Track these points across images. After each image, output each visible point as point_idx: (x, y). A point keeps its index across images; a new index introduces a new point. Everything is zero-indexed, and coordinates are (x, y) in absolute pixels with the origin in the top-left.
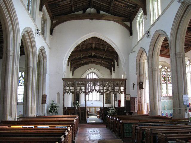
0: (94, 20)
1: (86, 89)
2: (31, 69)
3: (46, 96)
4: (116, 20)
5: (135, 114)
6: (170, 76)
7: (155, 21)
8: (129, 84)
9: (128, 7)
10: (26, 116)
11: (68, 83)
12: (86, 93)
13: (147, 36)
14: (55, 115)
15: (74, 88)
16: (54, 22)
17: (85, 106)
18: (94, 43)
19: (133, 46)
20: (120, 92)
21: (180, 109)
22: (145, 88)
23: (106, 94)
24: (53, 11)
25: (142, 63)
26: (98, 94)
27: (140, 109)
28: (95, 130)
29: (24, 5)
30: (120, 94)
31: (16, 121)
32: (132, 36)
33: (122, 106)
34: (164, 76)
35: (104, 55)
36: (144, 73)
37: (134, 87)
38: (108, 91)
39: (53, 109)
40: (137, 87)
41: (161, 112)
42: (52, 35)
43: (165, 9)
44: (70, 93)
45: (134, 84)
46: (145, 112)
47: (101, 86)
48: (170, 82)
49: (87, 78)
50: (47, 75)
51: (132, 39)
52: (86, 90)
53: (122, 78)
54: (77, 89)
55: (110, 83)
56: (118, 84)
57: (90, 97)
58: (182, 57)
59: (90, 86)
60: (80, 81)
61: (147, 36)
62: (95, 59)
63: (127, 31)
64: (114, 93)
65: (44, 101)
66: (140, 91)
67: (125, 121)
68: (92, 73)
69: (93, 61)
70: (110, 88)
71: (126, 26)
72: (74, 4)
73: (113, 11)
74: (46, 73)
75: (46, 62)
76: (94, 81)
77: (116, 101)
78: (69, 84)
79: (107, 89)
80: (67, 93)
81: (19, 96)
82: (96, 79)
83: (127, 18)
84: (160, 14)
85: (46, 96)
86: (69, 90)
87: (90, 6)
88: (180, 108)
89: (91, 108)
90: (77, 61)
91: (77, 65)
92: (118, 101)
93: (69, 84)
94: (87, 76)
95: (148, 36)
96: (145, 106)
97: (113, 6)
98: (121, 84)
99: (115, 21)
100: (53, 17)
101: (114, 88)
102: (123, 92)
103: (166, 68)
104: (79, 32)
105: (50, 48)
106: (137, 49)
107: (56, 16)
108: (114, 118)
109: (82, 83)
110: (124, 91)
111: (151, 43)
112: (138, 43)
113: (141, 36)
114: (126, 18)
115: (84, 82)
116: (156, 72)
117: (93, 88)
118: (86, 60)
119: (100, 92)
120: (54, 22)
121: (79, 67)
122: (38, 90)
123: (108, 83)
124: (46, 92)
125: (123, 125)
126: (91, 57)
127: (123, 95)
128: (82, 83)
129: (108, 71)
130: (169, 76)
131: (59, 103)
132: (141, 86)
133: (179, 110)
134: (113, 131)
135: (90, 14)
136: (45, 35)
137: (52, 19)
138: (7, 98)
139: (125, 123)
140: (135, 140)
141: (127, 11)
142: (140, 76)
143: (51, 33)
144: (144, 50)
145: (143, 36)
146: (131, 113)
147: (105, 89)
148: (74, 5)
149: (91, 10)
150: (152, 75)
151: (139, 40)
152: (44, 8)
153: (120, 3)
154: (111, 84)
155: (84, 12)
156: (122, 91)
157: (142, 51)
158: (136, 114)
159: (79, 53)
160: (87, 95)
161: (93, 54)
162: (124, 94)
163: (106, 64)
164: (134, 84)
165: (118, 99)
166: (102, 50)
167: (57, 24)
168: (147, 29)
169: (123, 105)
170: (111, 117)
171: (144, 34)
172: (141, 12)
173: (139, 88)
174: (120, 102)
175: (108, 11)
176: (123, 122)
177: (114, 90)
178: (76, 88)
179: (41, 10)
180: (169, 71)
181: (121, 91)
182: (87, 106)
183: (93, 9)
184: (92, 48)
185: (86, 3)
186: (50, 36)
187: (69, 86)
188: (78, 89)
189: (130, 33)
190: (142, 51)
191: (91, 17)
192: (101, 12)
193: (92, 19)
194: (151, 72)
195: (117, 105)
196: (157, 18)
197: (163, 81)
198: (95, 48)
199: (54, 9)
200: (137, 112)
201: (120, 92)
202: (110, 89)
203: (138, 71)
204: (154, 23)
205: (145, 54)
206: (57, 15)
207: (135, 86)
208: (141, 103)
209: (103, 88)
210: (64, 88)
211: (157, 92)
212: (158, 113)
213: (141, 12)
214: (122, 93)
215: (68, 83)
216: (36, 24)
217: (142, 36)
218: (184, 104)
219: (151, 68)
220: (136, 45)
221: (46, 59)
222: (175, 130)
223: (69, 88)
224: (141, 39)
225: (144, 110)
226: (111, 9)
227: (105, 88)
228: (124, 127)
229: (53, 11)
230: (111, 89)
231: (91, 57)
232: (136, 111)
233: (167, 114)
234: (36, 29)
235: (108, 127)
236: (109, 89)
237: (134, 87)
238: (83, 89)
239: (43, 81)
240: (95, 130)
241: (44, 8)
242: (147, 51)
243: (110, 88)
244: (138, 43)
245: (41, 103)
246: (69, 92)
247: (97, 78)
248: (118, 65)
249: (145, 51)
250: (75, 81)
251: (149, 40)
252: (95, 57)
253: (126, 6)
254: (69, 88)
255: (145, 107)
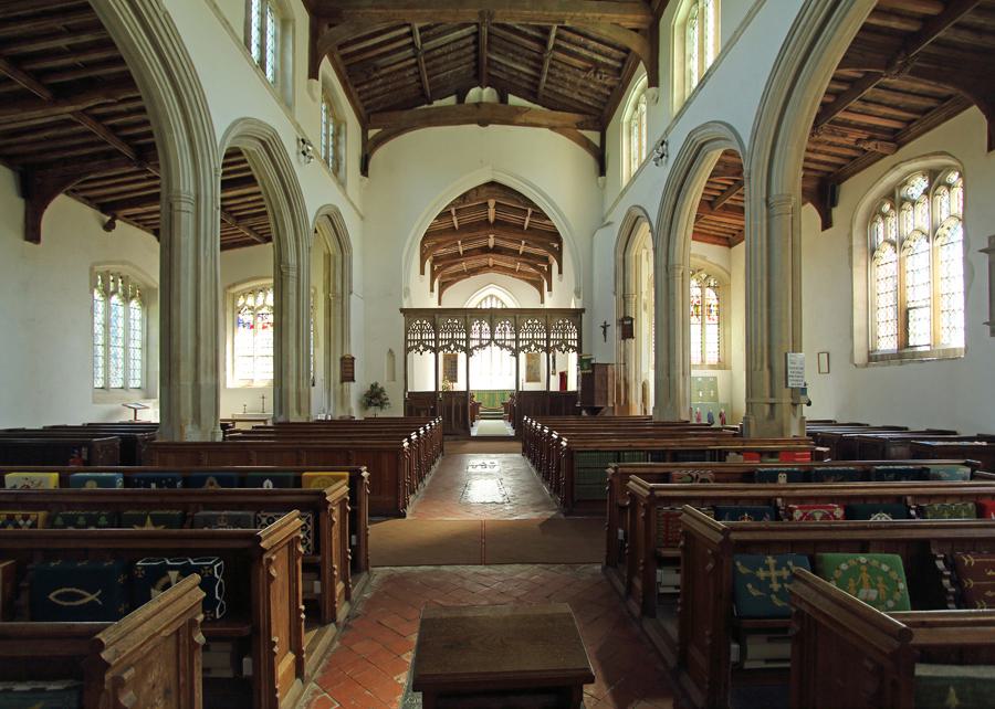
0: (490, 126)
2: (293, 273)
3: (353, 358)
4: (558, 123)
5: (606, 415)
7: (690, 98)
9: (595, 73)
10: (281, 419)
12: (469, 352)
13: (656, 160)
16: (372, 133)
17: (465, 389)
18: (492, 203)
19: (607, 209)
21: (772, 405)
22: (638, 335)
24: (366, 95)
26: (506, 353)
28: (488, 462)
29: (232, 32)
31: (218, 443)
35: (523, 242)
36: (638, 292)
37: (605, 332)
38: (530, 345)
39: (374, 396)
40: (614, 331)
42: (367, 176)
43: (738, 29)
44: (424, 350)
46: (636, 411)
50: (353, 297)
52: (467, 343)
53: (573, 307)
54: (442, 340)
56: (559, 325)
58: (790, 211)
59: (479, 330)
61: (656, 160)
62: (499, 256)
63: (589, 160)
64: (548, 350)
65: (348, 375)
67: (578, 446)
69: (494, 265)
71: (586, 144)
72: (427, 69)
73: (550, 90)
74: (351, 293)
75: (350, 258)
77: (554, 374)
79: (529, 340)
81: (122, 344)
83: (592, 119)
84: (710, 60)
85: (353, 358)
86: (421, 341)
87: (478, 79)
88: (773, 401)
89: (910, 312)
95: (661, 157)
97: (551, 66)
99: (552, 128)
100: (369, 116)
101: (548, 336)
102: (573, 347)
103: (704, 276)
104: (445, 161)
105: (362, 218)
106: (618, 217)
107: (377, 112)
108: (542, 428)
111: (668, 181)
112: (622, 195)
113: (635, 167)
114: (588, 117)
117: (488, 337)
118: (474, 262)
120: (372, 133)
123: (561, 322)
126: (485, 250)
127: (573, 357)
132: (628, 331)
133: (767, 408)
134: (539, 470)
135: (478, 105)
137: (365, 124)
138: (179, 365)
139: (578, 452)
140: (621, 531)
141: (592, 90)
142: (624, 298)
143: (364, 170)
144: (640, 213)
145: (642, 166)
146: (594, 411)
147: (523, 340)
148: (430, 72)
149: (481, 95)
150: (668, 294)
151: (625, 182)
152: (326, 66)
153: (571, 59)
155: (461, 100)
156: (571, 346)
157: (632, 225)
159: (452, 237)
165: (559, 369)
167: (379, 141)
168: (658, 137)
169: (572, 386)
171: (644, 157)
172: (641, 80)
173: (620, 336)
174: (564, 377)
175: (532, 95)
177: (548, 344)
179: (314, 73)
180: (712, 284)
183: (488, 89)
185: (465, 66)
187: (421, 330)
189: (598, 167)
190: (632, 225)
191: (483, 116)
192: (513, 100)
193: (483, 123)
195: (555, 386)
196: (695, 84)
199: (366, 87)
200: (613, 408)
201: (563, 347)
203: (620, 286)
204: (686, 104)
205: (645, 227)
206: (382, 111)
207: (608, 329)
208: (625, 379)
209: (517, 336)
213: (641, 80)
215: (418, 322)
216: (298, 119)
217: (637, 168)
218: (790, 384)
221: (350, 248)
222: (248, 209)
224: (633, 179)
225: (634, 402)
226: (541, 88)
229: (366, 95)
230: (540, 340)
231: (485, 250)
232: (610, 405)
233: (710, 416)
234: (298, 140)
235: (526, 451)
237: (605, 332)
238: (460, 340)
239: (342, 316)
241: (326, 66)
242: (654, 217)
244: (625, 190)
246: (421, 348)
247: (499, 307)
249: (647, 215)
250: (437, 316)
251: (663, 172)
252: (497, 250)
253: (587, 70)
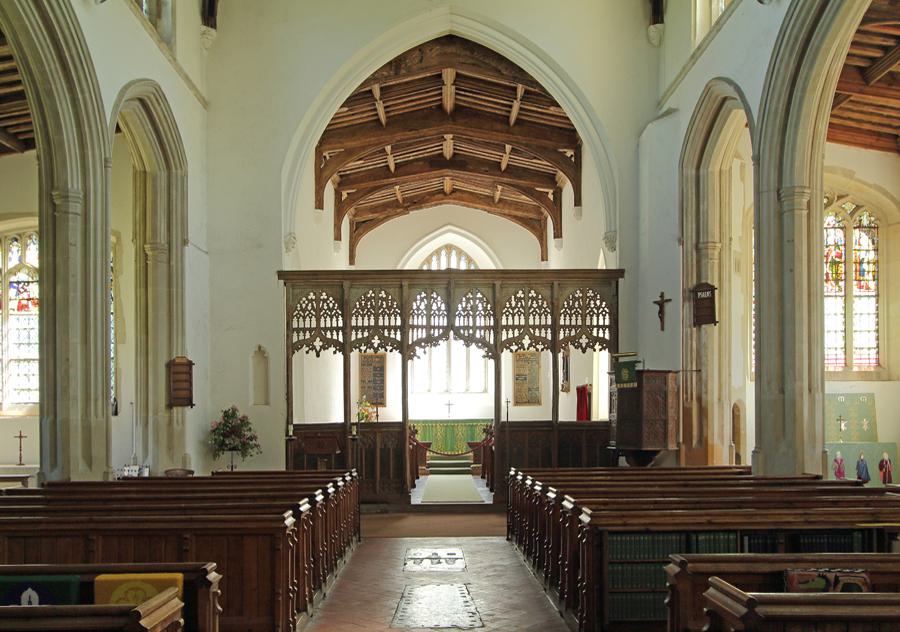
1: (404, 328)
3: (190, 364)
5: (664, 465)
6: (872, 256)
8: (638, 299)
10: (54, 476)
11: (312, 296)
14: (245, 465)
15: (404, 321)
18: (449, 75)
20: (584, 341)
22: (725, 316)
23: (519, 359)
25: (717, 174)
27: (695, 432)
28: (442, 553)
30: (584, 351)
32: (662, 22)
33: (594, 418)
34: (833, 254)
37: (661, 313)
38: (521, 337)
39: (230, 433)
40: (680, 311)
41: (825, 452)
42: (214, 26)
44: (323, 348)
45: (662, 296)
47: (439, 309)
48: (868, 288)
49: (434, 267)
51: (661, 42)
53: (601, 266)
55: (533, 294)
56: (575, 299)
57: (426, 362)
59: (428, 311)
60: (372, 287)
64: (554, 346)
65: (180, 389)
66: (699, 338)
68: (453, 239)
70: (531, 322)
74: (185, 242)
75: (184, 177)
76: (449, 284)
77: (567, 390)
78: (318, 300)
79: (519, 327)
80: (305, 348)
82: (458, 272)
86: (318, 331)
90: (371, 184)
91: (373, 210)
92: (574, 392)
93: (318, 300)
94: (434, 258)
96: (722, 417)
98: (594, 298)
101: (555, 321)
102: (602, 341)
106: (686, 100)
109: (383, 294)
110: (607, 337)
112: (694, 57)
115: (547, 292)
116: (805, 220)
117: (444, 322)
119: (483, 343)
121: (388, 218)
122: (143, 337)
123: (520, 294)
124: (189, 346)
125: (600, 546)
127: (602, 359)
128: (383, 294)
129: (530, 237)
130: (862, 255)
131: (267, 403)
132: (704, 311)
134: (538, 566)
136: (166, 21)
144: (730, 91)
146: (642, 458)
154: (386, 299)
158: (669, 463)
160: (411, 358)
161: (448, 149)
162: (605, 354)
163: (518, 206)
164: (662, 296)
166: (495, 118)
169: (601, 411)
170: (529, 482)
173: (690, 319)
174: (584, 396)
176: (604, 521)
177: (555, 334)
178: (354, 323)
181: (589, 336)
182: (412, 416)
184: (441, 107)
186: (204, 33)
188: (363, 328)
194: (774, 222)
195: (568, 413)
197: (837, 281)
198: (457, 108)
202: (534, 327)
205: (738, 117)
207: (668, 307)
208: (699, 400)
210: (289, 324)
211: (805, 338)
212: (807, 457)
214: (597, 347)
219: (773, 195)
220: (684, 71)
221: (183, 162)
223: (314, 325)
224: (717, 27)
227: (504, 322)
228: (608, 557)
230: (540, 327)
231: (437, 162)
232: (672, 447)
233: (861, 467)
235: (515, 533)
236: (527, 326)
237: (661, 313)
239: (170, 285)
240: (442, 553)
243: (531, 322)
244: (701, 49)
245: (163, 403)
246: (318, 343)
248: (578, 202)
250: (346, 284)
252: (458, 163)
254: (314, 325)
255: (722, 427)
